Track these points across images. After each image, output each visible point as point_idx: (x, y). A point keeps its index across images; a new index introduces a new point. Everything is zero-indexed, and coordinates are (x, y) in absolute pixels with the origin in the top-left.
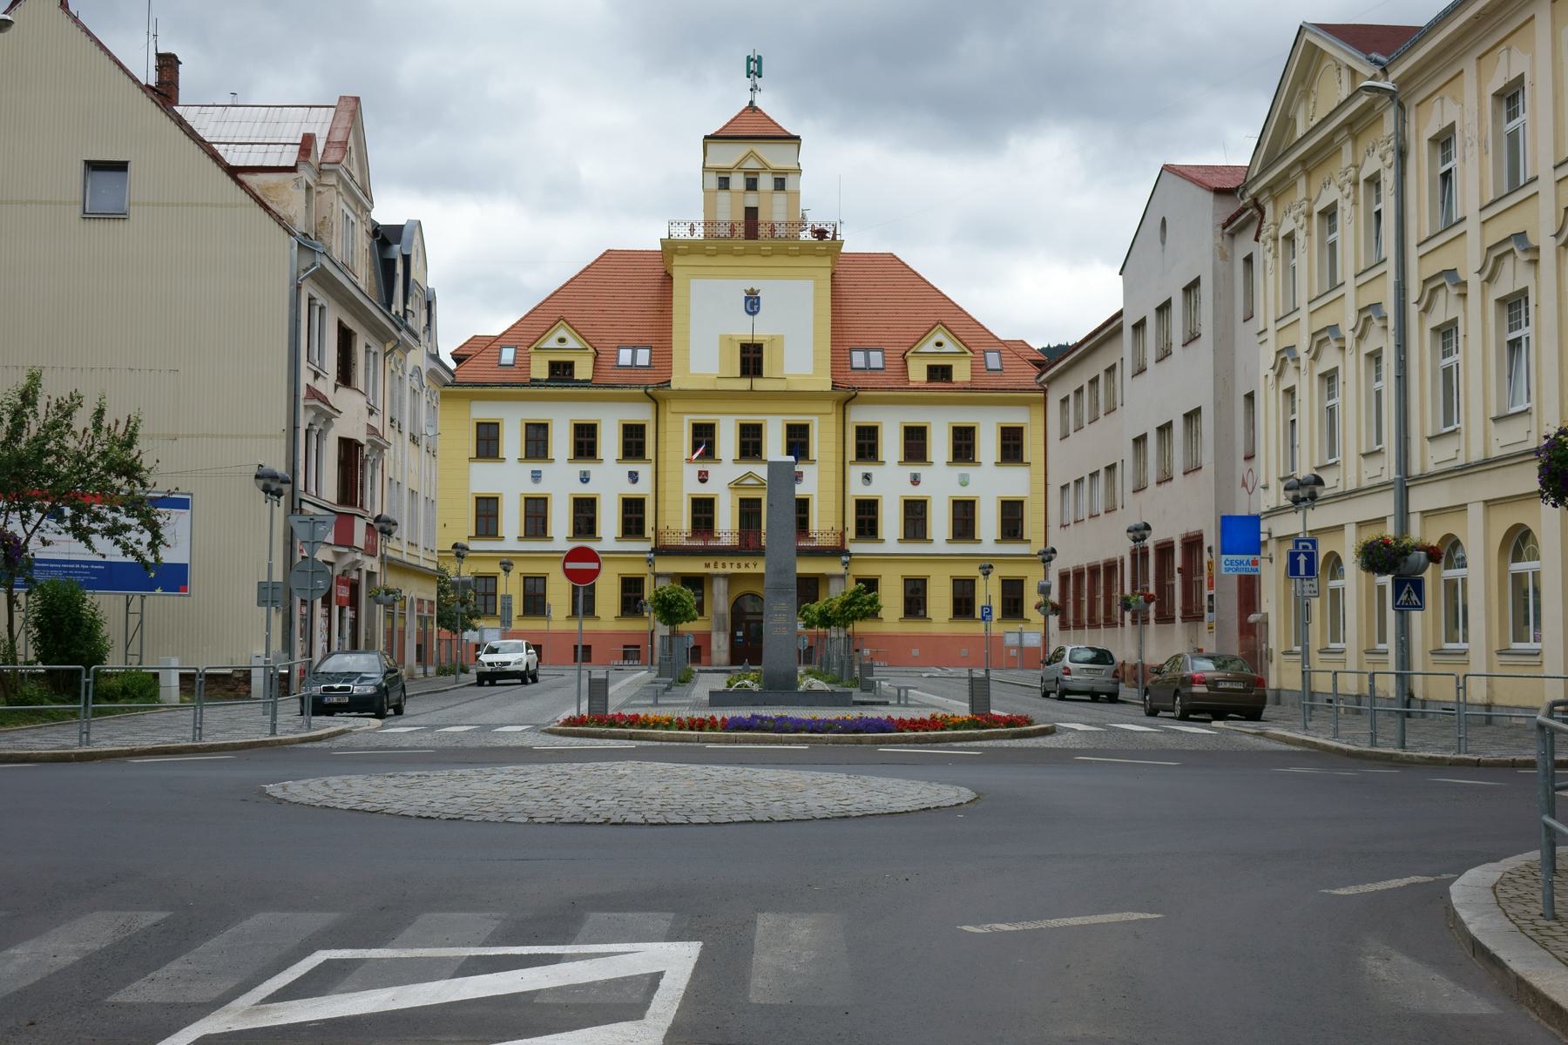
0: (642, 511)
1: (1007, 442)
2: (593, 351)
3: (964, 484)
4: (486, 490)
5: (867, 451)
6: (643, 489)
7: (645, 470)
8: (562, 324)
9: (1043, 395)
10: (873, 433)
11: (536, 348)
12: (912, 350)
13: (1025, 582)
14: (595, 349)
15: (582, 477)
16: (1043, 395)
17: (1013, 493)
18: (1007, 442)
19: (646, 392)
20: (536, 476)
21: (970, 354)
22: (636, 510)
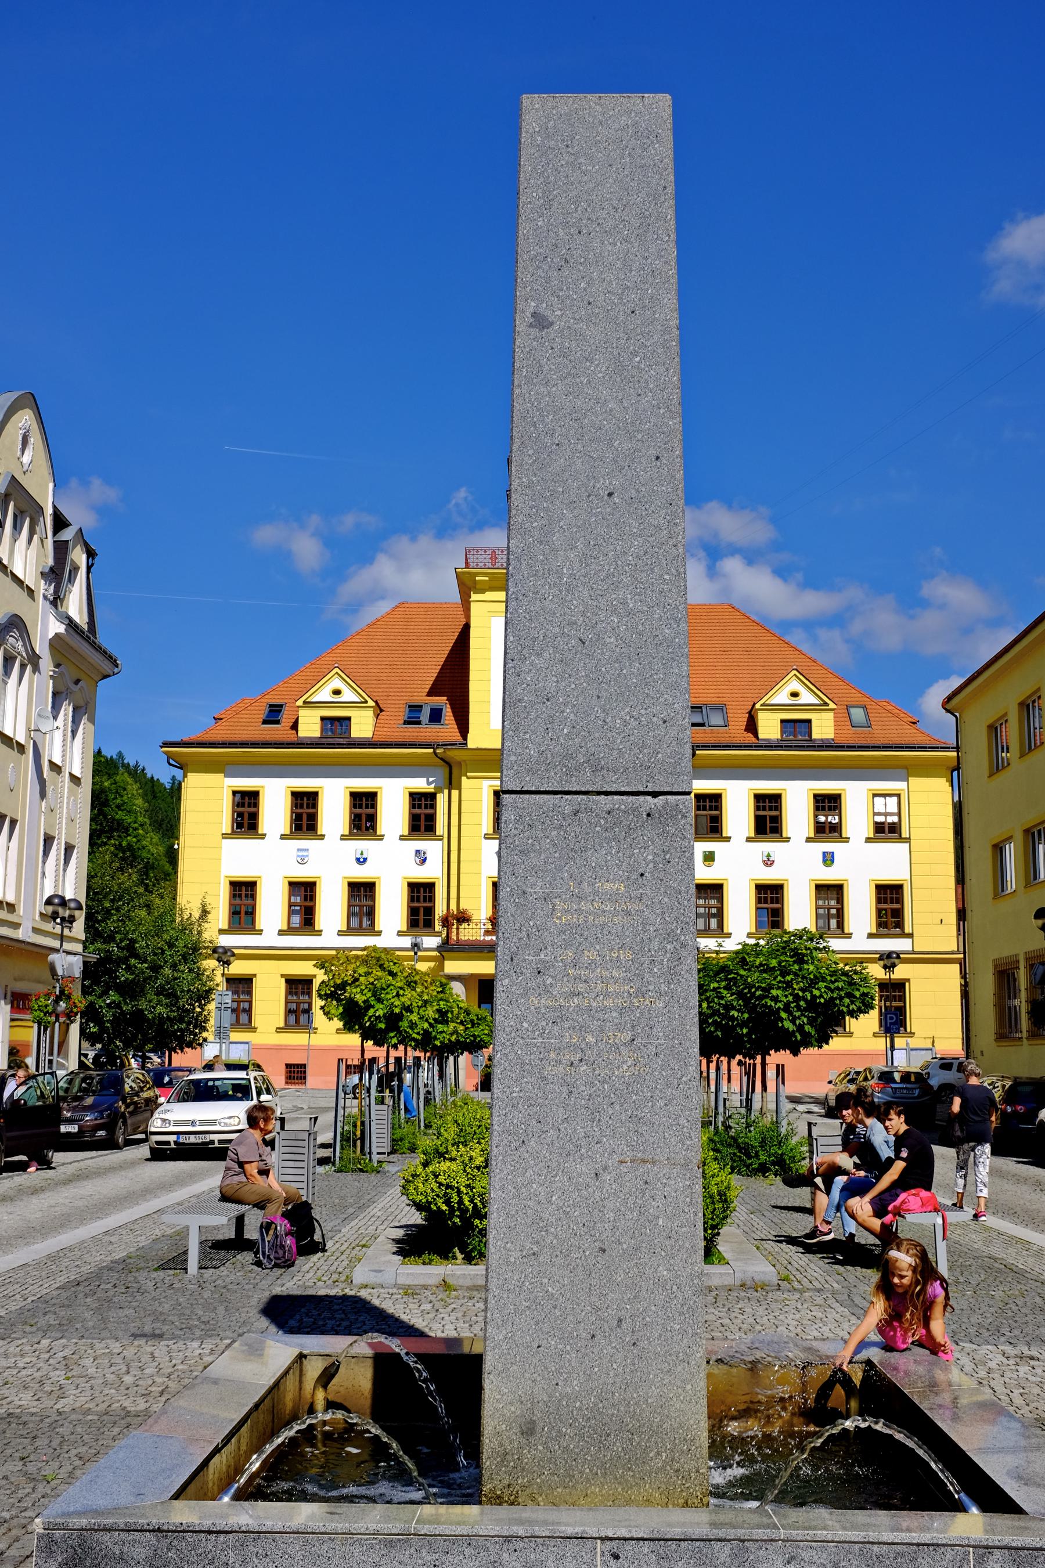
0: (431, 899)
1: (417, 811)
2: (373, 704)
3: (361, 861)
4: (243, 873)
5: (423, 823)
6: (432, 871)
7: (433, 849)
8: (337, 673)
9: (955, 754)
10: (717, 802)
11: (762, 705)
12: (762, 702)
13: (254, 979)
14: (376, 702)
15: (359, 856)
16: (955, 754)
17: (890, 875)
18: (417, 811)
19: (435, 752)
20: (828, 859)
21: (832, 706)
22: (425, 897)
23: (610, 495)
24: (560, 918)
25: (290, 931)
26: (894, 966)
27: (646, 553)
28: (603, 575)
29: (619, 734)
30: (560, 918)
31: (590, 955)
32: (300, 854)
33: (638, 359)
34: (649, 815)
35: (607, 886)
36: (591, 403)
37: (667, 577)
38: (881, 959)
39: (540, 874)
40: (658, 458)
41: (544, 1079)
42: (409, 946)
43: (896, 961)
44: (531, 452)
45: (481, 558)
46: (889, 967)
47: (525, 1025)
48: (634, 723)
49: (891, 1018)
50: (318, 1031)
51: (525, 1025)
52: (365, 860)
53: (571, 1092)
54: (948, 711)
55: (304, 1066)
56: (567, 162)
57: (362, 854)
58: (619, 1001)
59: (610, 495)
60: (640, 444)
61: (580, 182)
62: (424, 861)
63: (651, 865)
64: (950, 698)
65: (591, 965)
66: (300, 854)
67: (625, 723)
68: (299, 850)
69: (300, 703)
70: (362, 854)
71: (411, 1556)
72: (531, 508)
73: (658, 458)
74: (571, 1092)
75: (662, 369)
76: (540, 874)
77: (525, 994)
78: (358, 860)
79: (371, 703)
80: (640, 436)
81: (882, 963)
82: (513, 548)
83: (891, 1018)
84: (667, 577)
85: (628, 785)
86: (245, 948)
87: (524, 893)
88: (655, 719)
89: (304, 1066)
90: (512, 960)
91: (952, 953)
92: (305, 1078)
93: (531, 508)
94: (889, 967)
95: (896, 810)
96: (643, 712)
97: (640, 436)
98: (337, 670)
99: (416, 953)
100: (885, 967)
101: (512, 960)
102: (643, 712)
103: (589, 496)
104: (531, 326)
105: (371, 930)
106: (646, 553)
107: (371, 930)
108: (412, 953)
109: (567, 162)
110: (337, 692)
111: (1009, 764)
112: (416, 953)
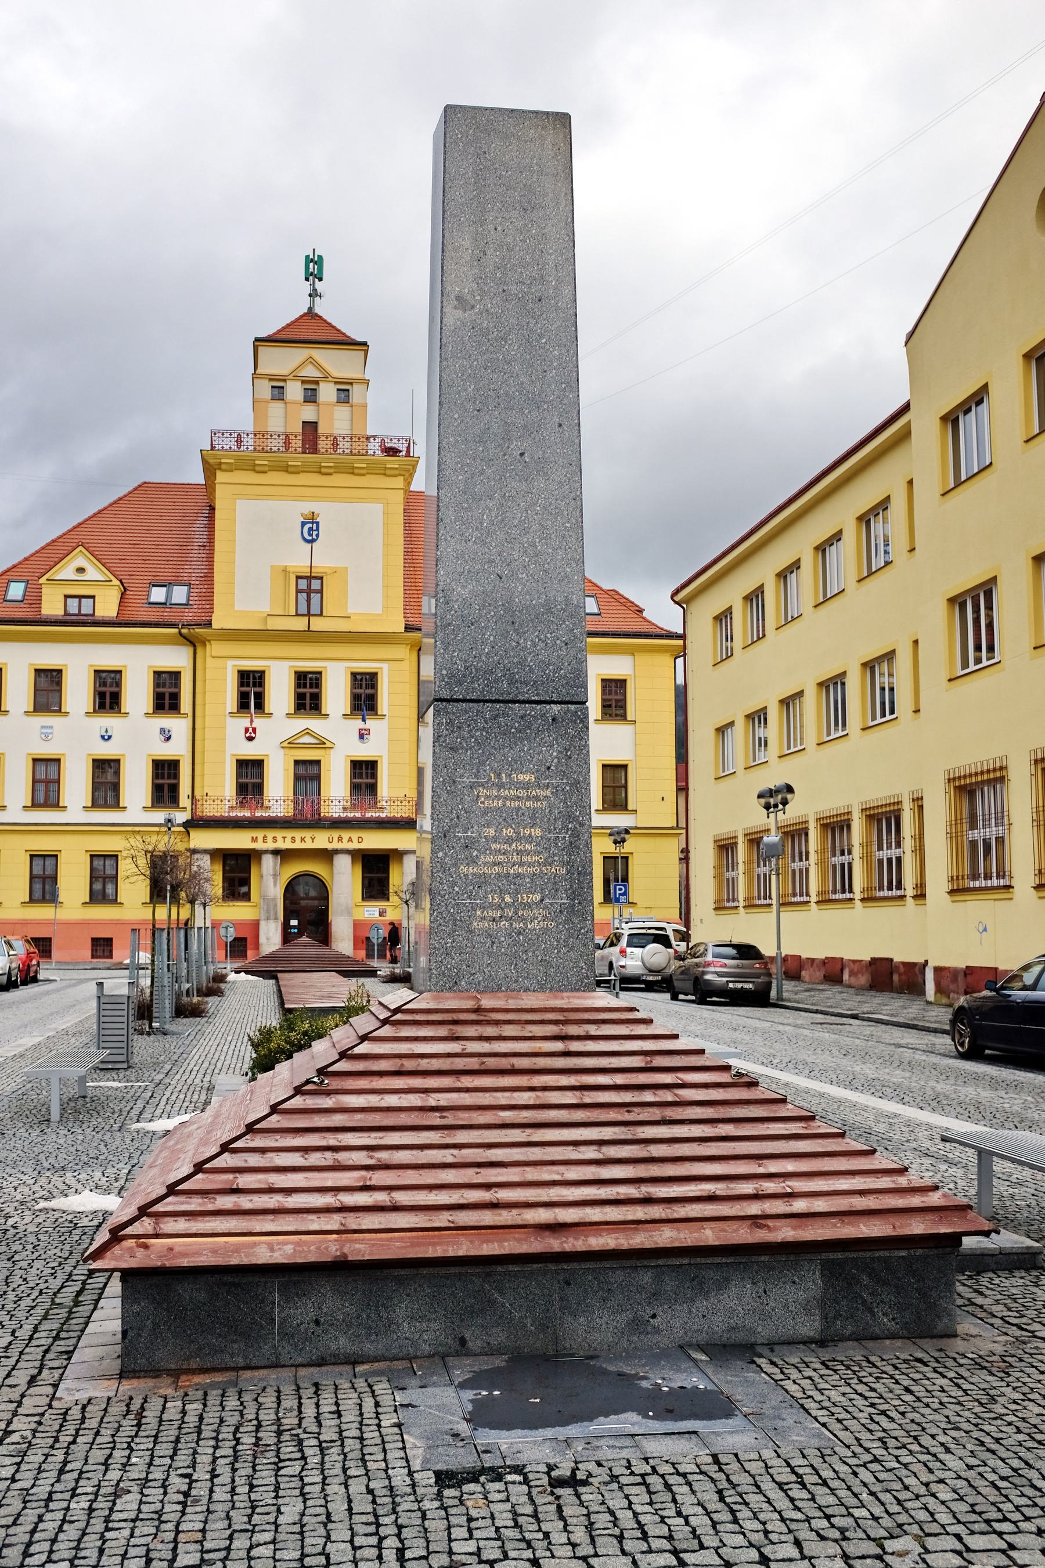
2: (118, 583)
3: (106, 738)
6: (177, 749)
7: (178, 725)
14: (121, 581)
15: (104, 733)
23: (522, 454)
24: (483, 803)
25: (35, 805)
26: (623, 841)
27: (551, 504)
28: (516, 522)
29: (530, 653)
30: (483, 803)
31: (508, 832)
32: (44, 731)
33: (544, 341)
34: (554, 720)
35: (521, 777)
36: (506, 377)
37: (568, 525)
38: (610, 835)
39: (467, 767)
40: (560, 425)
41: (471, 932)
42: (163, 822)
43: (627, 836)
44: (456, 416)
45: (227, 441)
46: (619, 842)
47: (457, 889)
48: (542, 645)
49: (620, 889)
50: (64, 905)
51: (457, 889)
52: (110, 737)
53: (493, 943)
54: (676, 603)
55: (50, 939)
56: (485, 167)
57: (107, 731)
58: (531, 870)
59: (522, 454)
60: (546, 412)
61: (495, 185)
62: (168, 739)
63: (556, 760)
64: (677, 592)
65: (509, 841)
66: (44, 731)
67: (535, 645)
68: (43, 727)
69: (43, 580)
70: (107, 731)
71: (415, 1290)
72: (457, 463)
73: (560, 425)
74: (493, 943)
75: (564, 351)
76: (467, 767)
77: (456, 865)
78: (103, 737)
79: (116, 582)
80: (545, 407)
81: (612, 838)
82: (442, 497)
83: (620, 889)
84: (568, 525)
85: (537, 695)
86: (113, 825)
87: (454, 782)
88: (558, 642)
89: (50, 939)
90: (445, 836)
91: (672, 828)
92: (50, 951)
93: (457, 463)
94: (619, 842)
95: (77, 600)
96: (549, 635)
97: (545, 407)
98: (81, 548)
99: (169, 829)
100: (615, 842)
101: (445, 836)
102: (549, 635)
103: (504, 455)
104: (455, 308)
105: (116, 804)
106: (551, 504)
107: (116, 804)
108: (166, 829)
109: (485, 167)
110: (81, 570)
111: (732, 655)
112: (169, 829)
